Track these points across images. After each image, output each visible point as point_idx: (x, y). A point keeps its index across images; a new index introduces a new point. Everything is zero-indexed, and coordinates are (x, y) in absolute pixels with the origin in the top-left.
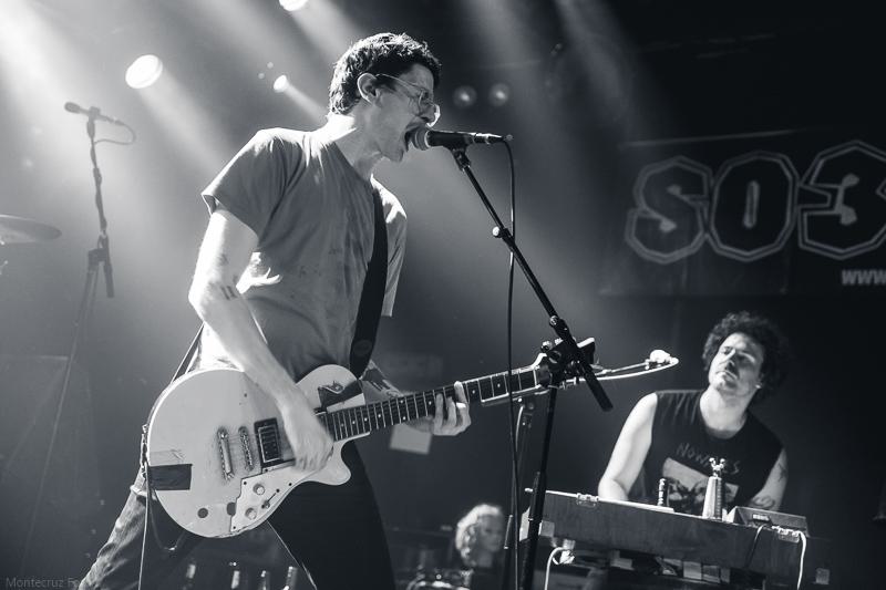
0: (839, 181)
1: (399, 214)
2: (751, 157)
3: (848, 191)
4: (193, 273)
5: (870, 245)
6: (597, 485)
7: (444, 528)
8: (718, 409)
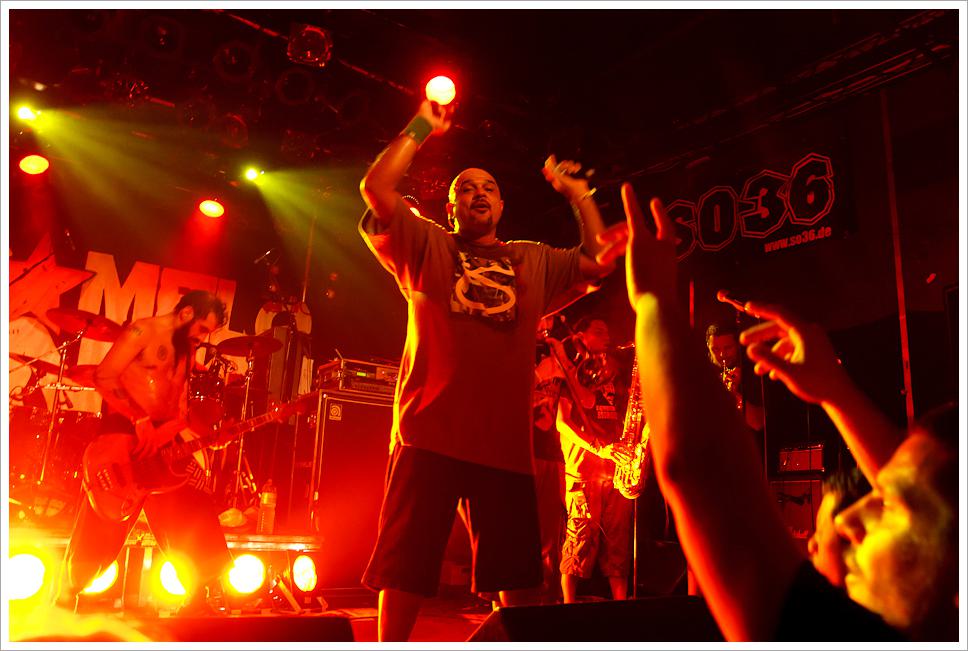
1: (231, 328)
2: (773, 229)
5: (781, 223)
8: (252, 477)
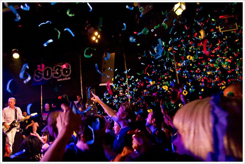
0: (56, 70)
5: (61, 76)
6: (28, 105)
7: (195, 65)
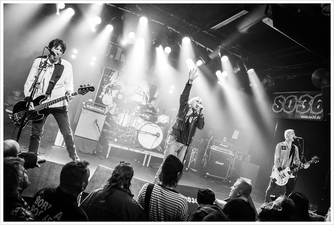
0: (303, 101)
3: (304, 103)
4: (319, 5)
